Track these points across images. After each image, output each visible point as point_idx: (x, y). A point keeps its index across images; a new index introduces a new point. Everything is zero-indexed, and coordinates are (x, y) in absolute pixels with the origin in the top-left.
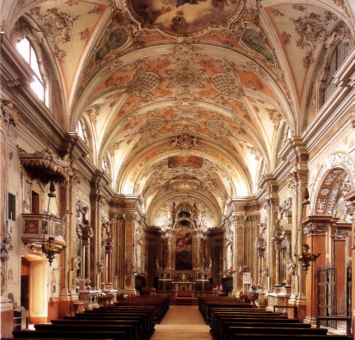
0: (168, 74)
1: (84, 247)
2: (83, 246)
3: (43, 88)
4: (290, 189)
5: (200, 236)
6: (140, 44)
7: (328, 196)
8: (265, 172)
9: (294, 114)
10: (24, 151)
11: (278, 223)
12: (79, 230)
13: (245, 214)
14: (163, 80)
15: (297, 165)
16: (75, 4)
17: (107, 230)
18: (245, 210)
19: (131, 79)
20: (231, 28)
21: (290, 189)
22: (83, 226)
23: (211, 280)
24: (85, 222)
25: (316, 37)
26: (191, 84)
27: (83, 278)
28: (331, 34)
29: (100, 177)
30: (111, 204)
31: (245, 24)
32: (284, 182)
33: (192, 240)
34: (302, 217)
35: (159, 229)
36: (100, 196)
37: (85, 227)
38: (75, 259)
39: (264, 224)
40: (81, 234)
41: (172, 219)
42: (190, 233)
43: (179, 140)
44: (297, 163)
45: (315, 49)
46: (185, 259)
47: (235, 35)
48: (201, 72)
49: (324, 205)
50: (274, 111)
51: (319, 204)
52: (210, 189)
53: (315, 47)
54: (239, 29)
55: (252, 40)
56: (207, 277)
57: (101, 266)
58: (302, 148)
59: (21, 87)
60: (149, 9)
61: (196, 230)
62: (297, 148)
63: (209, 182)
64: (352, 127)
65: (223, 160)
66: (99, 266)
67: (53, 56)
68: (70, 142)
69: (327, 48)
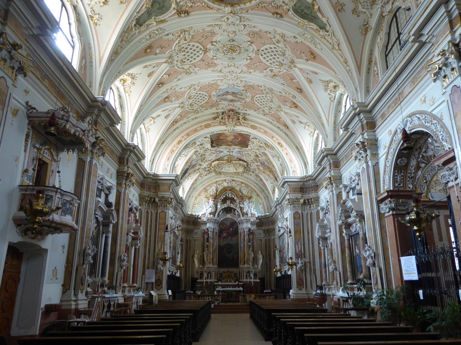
0: (213, 45)
1: (104, 236)
2: (102, 235)
3: (72, 50)
4: (357, 161)
5: (246, 226)
6: (184, 13)
7: (407, 166)
8: (322, 146)
9: (354, 81)
10: (34, 109)
11: (344, 203)
12: (99, 213)
13: (302, 197)
14: (208, 52)
15: (363, 134)
17: (135, 216)
18: (301, 192)
19: (173, 49)
21: (357, 161)
22: (105, 208)
23: (262, 280)
24: (108, 204)
25: (372, 5)
27: (98, 277)
29: (131, 151)
30: (142, 185)
32: (348, 158)
33: (238, 230)
34: (377, 193)
35: (198, 218)
36: (128, 174)
37: (107, 211)
38: (89, 249)
39: (325, 207)
40: (101, 219)
41: (214, 205)
42: (236, 222)
43: (223, 116)
44: (363, 131)
46: (229, 253)
47: (285, 6)
48: (249, 43)
49: (402, 177)
50: (328, 82)
51: (397, 176)
52: (257, 172)
53: (371, 15)
55: (304, 10)
56: (257, 276)
57: (124, 260)
58: (333, 157)
59: (42, 38)
61: (243, 218)
62: (362, 116)
63: (256, 163)
64: (433, 81)
65: (273, 137)
66: (121, 260)
69: (385, 15)
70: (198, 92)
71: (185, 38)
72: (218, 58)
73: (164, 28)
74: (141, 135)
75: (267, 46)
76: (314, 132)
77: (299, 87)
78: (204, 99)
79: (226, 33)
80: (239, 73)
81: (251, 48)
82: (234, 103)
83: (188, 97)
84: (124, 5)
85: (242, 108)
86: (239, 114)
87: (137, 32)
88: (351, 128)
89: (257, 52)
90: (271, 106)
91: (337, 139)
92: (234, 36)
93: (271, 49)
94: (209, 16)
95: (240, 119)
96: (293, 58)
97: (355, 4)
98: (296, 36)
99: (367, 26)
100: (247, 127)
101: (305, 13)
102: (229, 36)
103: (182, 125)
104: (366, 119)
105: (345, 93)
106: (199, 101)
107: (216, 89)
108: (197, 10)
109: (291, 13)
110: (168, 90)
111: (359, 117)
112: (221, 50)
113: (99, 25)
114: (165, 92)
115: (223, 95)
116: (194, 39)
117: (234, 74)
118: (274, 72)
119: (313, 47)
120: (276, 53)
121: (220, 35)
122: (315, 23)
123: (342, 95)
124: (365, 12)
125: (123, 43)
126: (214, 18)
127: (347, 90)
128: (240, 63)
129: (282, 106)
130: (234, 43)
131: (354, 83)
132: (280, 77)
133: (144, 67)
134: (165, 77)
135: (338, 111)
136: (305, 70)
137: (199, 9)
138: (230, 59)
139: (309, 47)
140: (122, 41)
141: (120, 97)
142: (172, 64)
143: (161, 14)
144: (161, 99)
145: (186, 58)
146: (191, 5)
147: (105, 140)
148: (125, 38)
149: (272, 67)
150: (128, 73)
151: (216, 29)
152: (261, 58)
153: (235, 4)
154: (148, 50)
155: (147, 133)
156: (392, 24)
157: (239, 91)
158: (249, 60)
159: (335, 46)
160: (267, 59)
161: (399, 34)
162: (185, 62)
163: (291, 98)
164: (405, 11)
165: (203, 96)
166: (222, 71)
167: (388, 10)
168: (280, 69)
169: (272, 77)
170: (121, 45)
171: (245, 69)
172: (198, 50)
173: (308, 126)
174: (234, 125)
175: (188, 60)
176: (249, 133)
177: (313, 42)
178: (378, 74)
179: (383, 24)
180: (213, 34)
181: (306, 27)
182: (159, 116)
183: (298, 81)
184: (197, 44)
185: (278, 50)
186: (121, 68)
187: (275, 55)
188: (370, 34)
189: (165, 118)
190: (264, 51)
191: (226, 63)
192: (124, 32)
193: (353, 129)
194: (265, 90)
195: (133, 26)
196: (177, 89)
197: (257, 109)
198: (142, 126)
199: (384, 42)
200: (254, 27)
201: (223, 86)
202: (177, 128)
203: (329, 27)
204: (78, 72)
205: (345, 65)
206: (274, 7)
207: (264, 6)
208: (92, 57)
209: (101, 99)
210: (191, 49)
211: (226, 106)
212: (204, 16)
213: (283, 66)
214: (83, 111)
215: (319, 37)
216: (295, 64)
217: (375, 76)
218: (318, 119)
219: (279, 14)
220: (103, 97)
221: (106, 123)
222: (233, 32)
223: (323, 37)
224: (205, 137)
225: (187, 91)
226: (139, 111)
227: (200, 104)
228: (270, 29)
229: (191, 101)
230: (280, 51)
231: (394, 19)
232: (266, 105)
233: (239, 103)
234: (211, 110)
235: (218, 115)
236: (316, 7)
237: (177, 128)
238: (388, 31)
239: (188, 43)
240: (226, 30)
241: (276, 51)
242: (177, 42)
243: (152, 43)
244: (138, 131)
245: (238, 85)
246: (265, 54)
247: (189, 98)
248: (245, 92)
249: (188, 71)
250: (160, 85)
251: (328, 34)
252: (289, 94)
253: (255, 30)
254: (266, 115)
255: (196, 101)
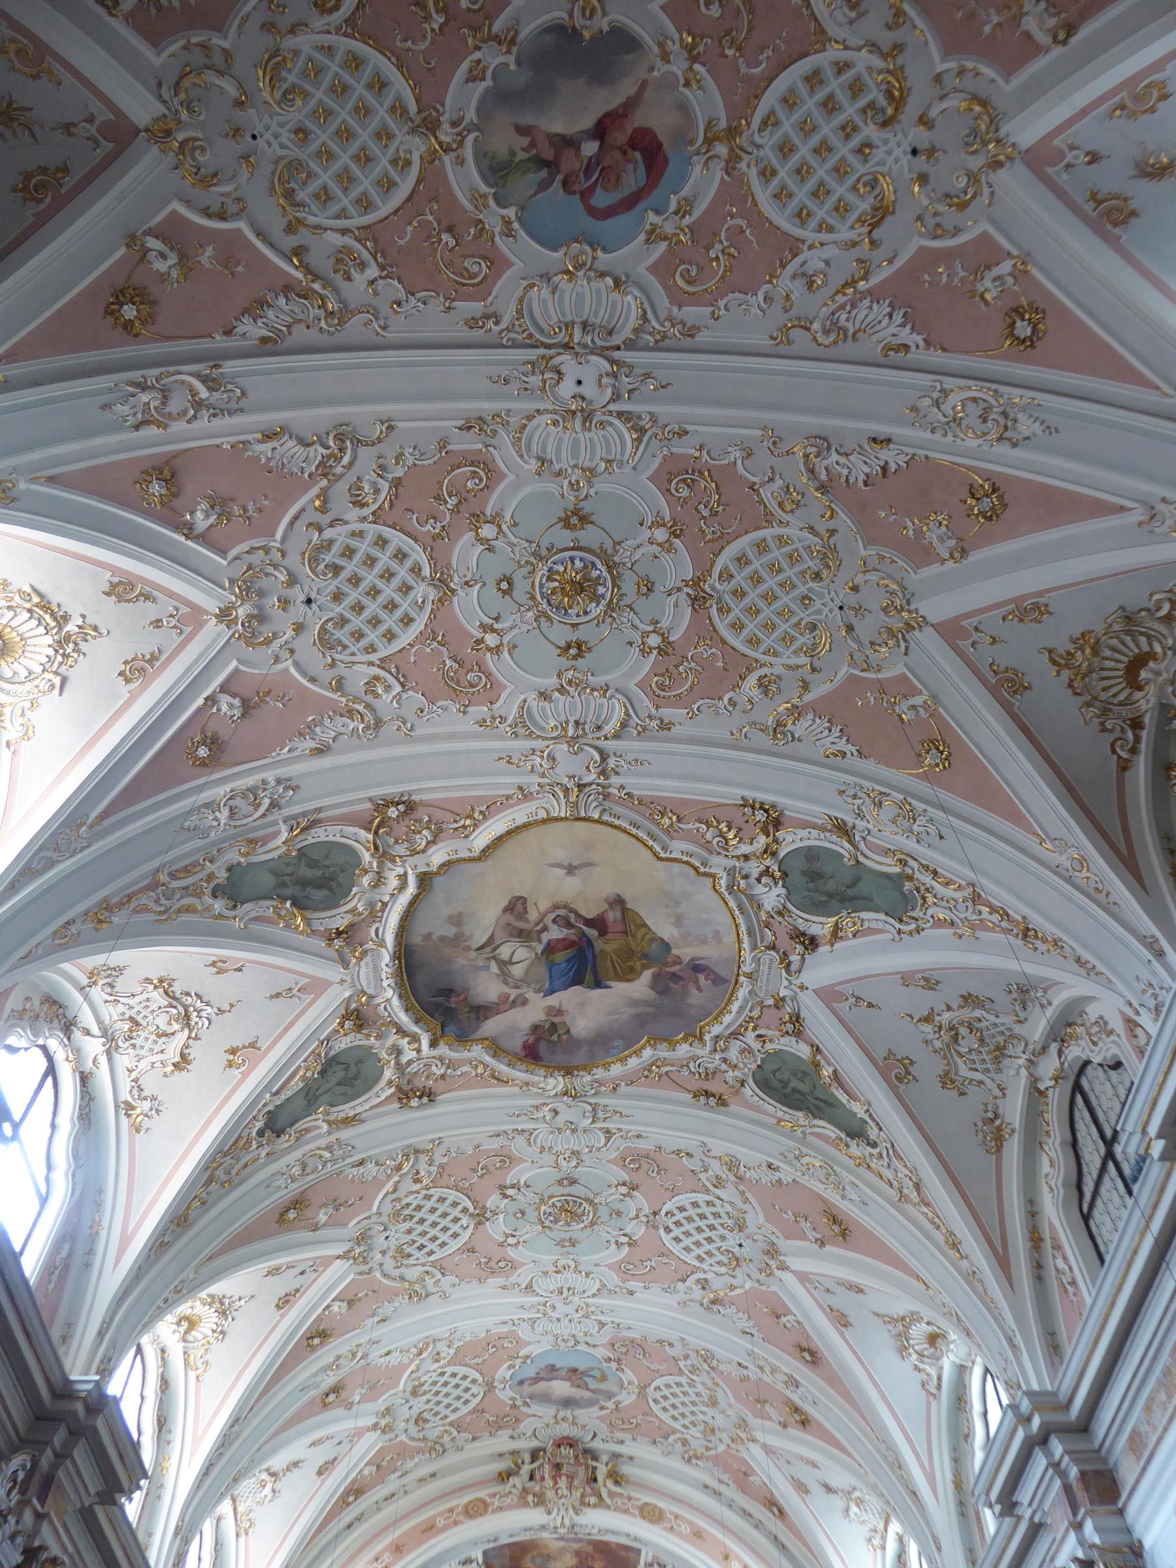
0: (505, 1196)
3: (37, 1207)
6: (420, 1097)
9: (996, 1312)
14: (488, 1220)
16: (235, 970)
19: (374, 1210)
20: (715, 1050)
25: (997, 1060)
26: (588, 1231)
28: (1044, 1049)
31: (759, 1036)
43: (536, 1465)
44: (1075, 1514)
45: (1004, 1094)
48: (624, 1190)
50: (905, 1321)
53: (1002, 1089)
54: (742, 1052)
60: (461, 997)
62: (1057, 1447)
67: (117, 1112)
68: (60, 1420)
69: (1047, 1089)
70: (449, 1370)
71: (418, 1173)
72: (521, 1240)
73: (352, 1142)
74: (218, 1546)
75: (683, 1199)
76: (886, 1530)
77: (805, 1344)
78: (467, 1396)
79: (549, 1158)
80: (594, 1295)
81: (631, 1207)
82: (577, 1412)
83: (409, 1389)
84: (237, 1073)
85: (604, 1431)
86: (595, 1458)
87: (264, 1154)
88: (1026, 1502)
89: (651, 1217)
90: (711, 1422)
91: (981, 1554)
92: (576, 1167)
93: (698, 1206)
94: (495, 1104)
95: (600, 1478)
96: (775, 1241)
97: (945, 1057)
98: (776, 1163)
99: (998, 1122)
100: (626, 1511)
101: (794, 1090)
102: (557, 1166)
103: (377, 1507)
104: (1076, 1461)
105: (973, 1363)
106: (448, 1406)
107: (511, 1358)
108: (462, 1087)
109: (750, 1091)
110: (341, 1361)
111: (1049, 1454)
112: (532, 1215)
113: (147, 1130)
114: (328, 1367)
115: (537, 1380)
116: (445, 1175)
117: (576, 1299)
118: (714, 1288)
119: (834, 1197)
120: (716, 1222)
121: (529, 1164)
122: (830, 1120)
123: (962, 1371)
124: (982, 1082)
125: (213, 1187)
126: (511, 1112)
127: (979, 1346)
128: (596, 1257)
129: (750, 1419)
130: (576, 1190)
131: (999, 1320)
132: (733, 1309)
133: (269, 1273)
134: (335, 1308)
135: (960, 1437)
136: (818, 1278)
137: (467, 1082)
138: (560, 1243)
139: (821, 1197)
140: (210, 1180)
141: (165, 1384)
142: (365, 1262)
143: (348, 1098)
144: (313, 1393)
145: (414, 1242)
146: (442, 1071)
147: (63, 1563)
148: (220, 1173)
149: (705, 1272)
150: (210, 1296)
151: (518, 1146)
152: (666, 1239)
153: (577, 1068)
154: (292, 1215)
155: (242, 1539)
156: (1077, 1114)
157: (595, 1364)
158: (626, 1249)
159: (905, 1191)
160: (687, 1242)
161: (1110, 1143)
162: (409, 1256)
163: (780, 1386)
164: (1105, 1071)
165: (465, 1384)
166: (535, 1287)
167: (1051, 1072)
168: (734, 1277)
169: (708, 1309)
170: (204, 1195)
171: (613, 1279)
172: (456, 1212)
173: (858, 1506)
174: (577, 1503)
175: (422, 1247)
176: (636, 1539)
177: (832, 1178)
178: (1073, 1283)
179: (1046, 1115)
180: (507, 1159)
181: (803, 1132)
182: (296, 1464)
183: (800, 1319)
184: (452, 1195)
185: (718, 1209)
186: (189, 1273)
187: (712, 1227)
188: (1013, 1148)
189: (320, 1473)
190: (673, 1215)
191: (547, 1259)
192: (221, 1152)
193: (1035, 1505)
194: (686, 1357)
195: (254, 1134)
196: (374, 1356)
197: (659, 1436)
198: (225, 1507)
199: (1066, 1172)
200: (638, 1136)
201: (538, 1345)
202: (360, 1518)
203: (876, 1130)
204: (33, 1289)
205: (953, 1254)
206: (697, 1076)
207: (667, 1073)
208: (97, 1233)
209: (89, 1387)
210: (433, 1210)
211: (548, 1425)
212: (483, 1104)
213: (743, 1264)
214: (13, 1435)
215: (851, 1163)
216: (781, 1258)
217: (1066, 1291)
218: (892, 1469)
219: (713, 1095)
220: (97, 1378)
221: (86, 1487)
222: (573, 1153)
223: (863, 1163)
224: (463, 1557)
225: (408, 1366)
226: (225, 1441)
227: (452, 1417)
228: (689, 1142)
229: (419, 1404)
230: (728, 1213)
231: (1079, 1099)
232: (692, 1418)
233: (594, 1411)
234: (493, 1441)
235: (516, 1464)
236: (826, 1072)
237: (360, 1518)
238: (1069, 1137)
239: (424, 1192)
240: (551, 1148)
241: (683, 1393)
242: (389, 1186)
243: (303, 1192)
244: (208, 1527)
245: (588, 1339)
246: (678, 1224)
247: (414, 1393)
248: (614, 1365)
249: (417, 1287)
250: (316, 1341)
251: (875, 1151)
252: (774, 1370)
253: (641, 1145)
254: (694, 1461)
255: (438, 1403)
